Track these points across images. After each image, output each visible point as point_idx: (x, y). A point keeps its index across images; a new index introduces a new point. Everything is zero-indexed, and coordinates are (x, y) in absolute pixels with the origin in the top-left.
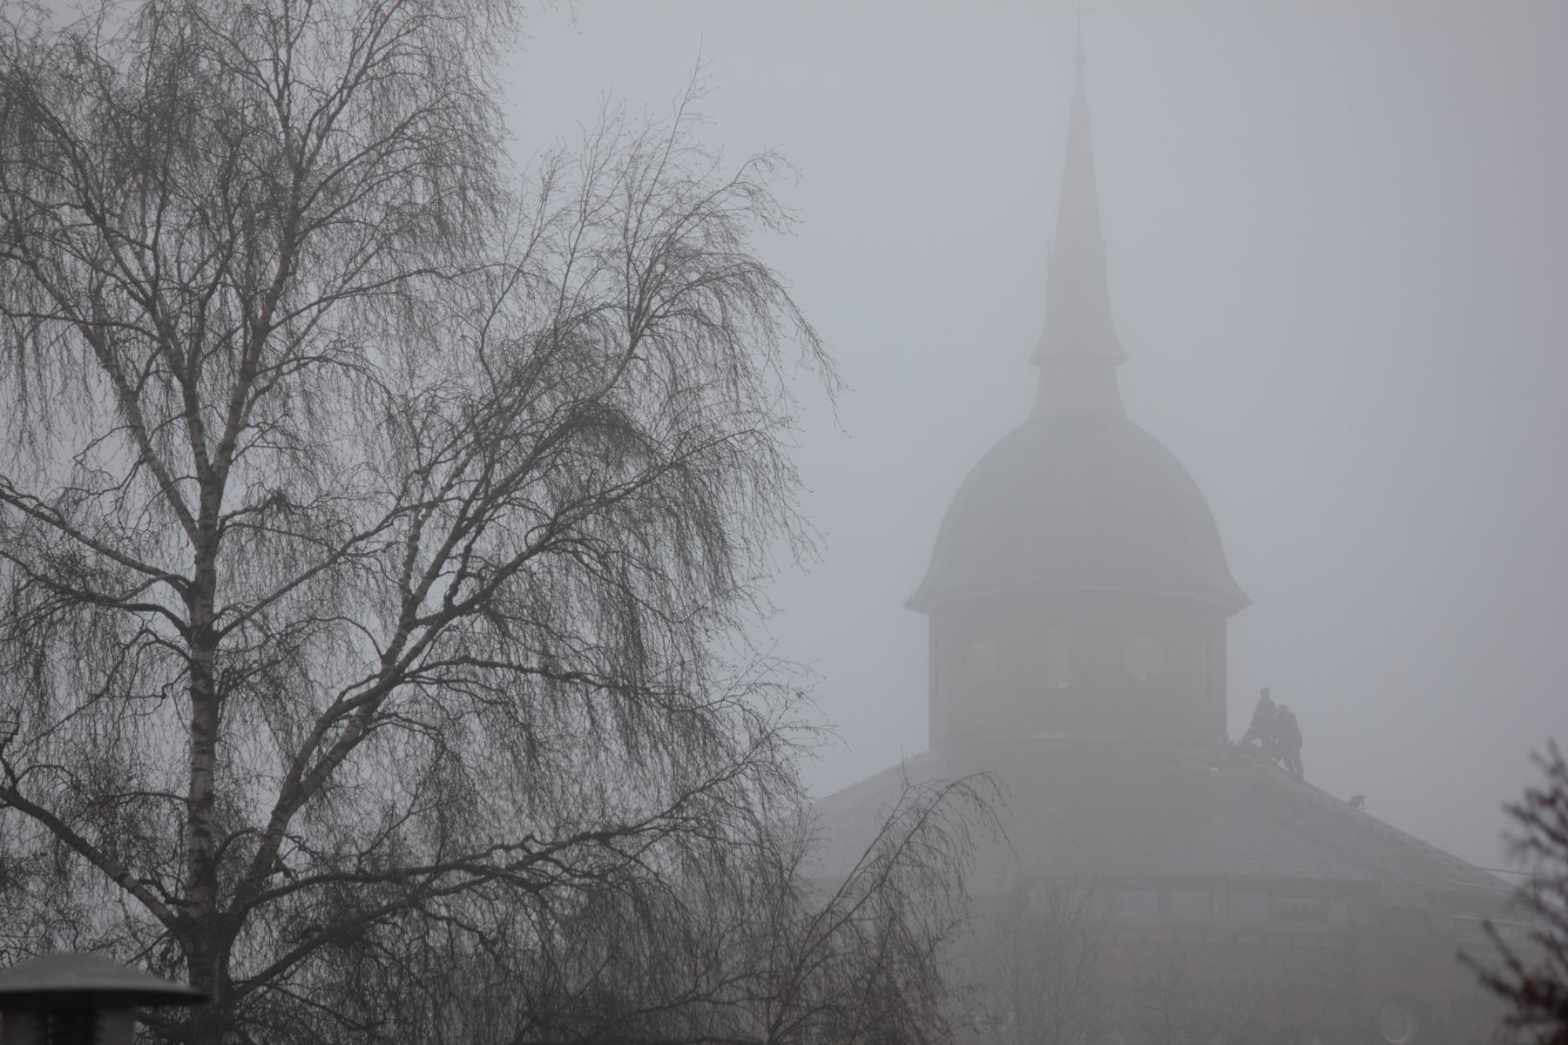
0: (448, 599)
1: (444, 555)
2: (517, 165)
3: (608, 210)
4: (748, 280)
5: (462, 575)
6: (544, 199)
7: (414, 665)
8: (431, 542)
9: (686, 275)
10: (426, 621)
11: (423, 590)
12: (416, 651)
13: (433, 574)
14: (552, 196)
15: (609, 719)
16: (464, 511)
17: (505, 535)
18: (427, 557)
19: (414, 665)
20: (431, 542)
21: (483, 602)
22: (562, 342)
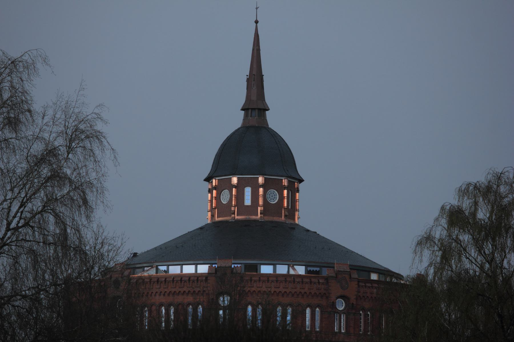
0: (17, 225)
1: (17, 212)
2: (37, 107)
3: (60, 121)
4: (97, 136)
5: (20, 218)
6: (43, 118)
7: (8, 241)
8: (15, 208)
9: (82, 135)
10: (13, 229)
11: (12, 221)
12: (9, 238)
13: (14, 217)
14: (45, 117)
15: (473, 251)
16: (23, 200)
17: (37, 204)
18: (12, 214)
19: (8, 241)
20: (15, 208)
21: (26, 224)
22: (51, 152)
